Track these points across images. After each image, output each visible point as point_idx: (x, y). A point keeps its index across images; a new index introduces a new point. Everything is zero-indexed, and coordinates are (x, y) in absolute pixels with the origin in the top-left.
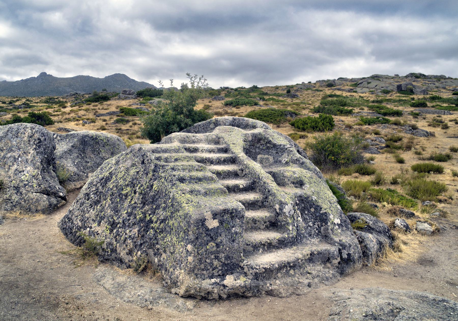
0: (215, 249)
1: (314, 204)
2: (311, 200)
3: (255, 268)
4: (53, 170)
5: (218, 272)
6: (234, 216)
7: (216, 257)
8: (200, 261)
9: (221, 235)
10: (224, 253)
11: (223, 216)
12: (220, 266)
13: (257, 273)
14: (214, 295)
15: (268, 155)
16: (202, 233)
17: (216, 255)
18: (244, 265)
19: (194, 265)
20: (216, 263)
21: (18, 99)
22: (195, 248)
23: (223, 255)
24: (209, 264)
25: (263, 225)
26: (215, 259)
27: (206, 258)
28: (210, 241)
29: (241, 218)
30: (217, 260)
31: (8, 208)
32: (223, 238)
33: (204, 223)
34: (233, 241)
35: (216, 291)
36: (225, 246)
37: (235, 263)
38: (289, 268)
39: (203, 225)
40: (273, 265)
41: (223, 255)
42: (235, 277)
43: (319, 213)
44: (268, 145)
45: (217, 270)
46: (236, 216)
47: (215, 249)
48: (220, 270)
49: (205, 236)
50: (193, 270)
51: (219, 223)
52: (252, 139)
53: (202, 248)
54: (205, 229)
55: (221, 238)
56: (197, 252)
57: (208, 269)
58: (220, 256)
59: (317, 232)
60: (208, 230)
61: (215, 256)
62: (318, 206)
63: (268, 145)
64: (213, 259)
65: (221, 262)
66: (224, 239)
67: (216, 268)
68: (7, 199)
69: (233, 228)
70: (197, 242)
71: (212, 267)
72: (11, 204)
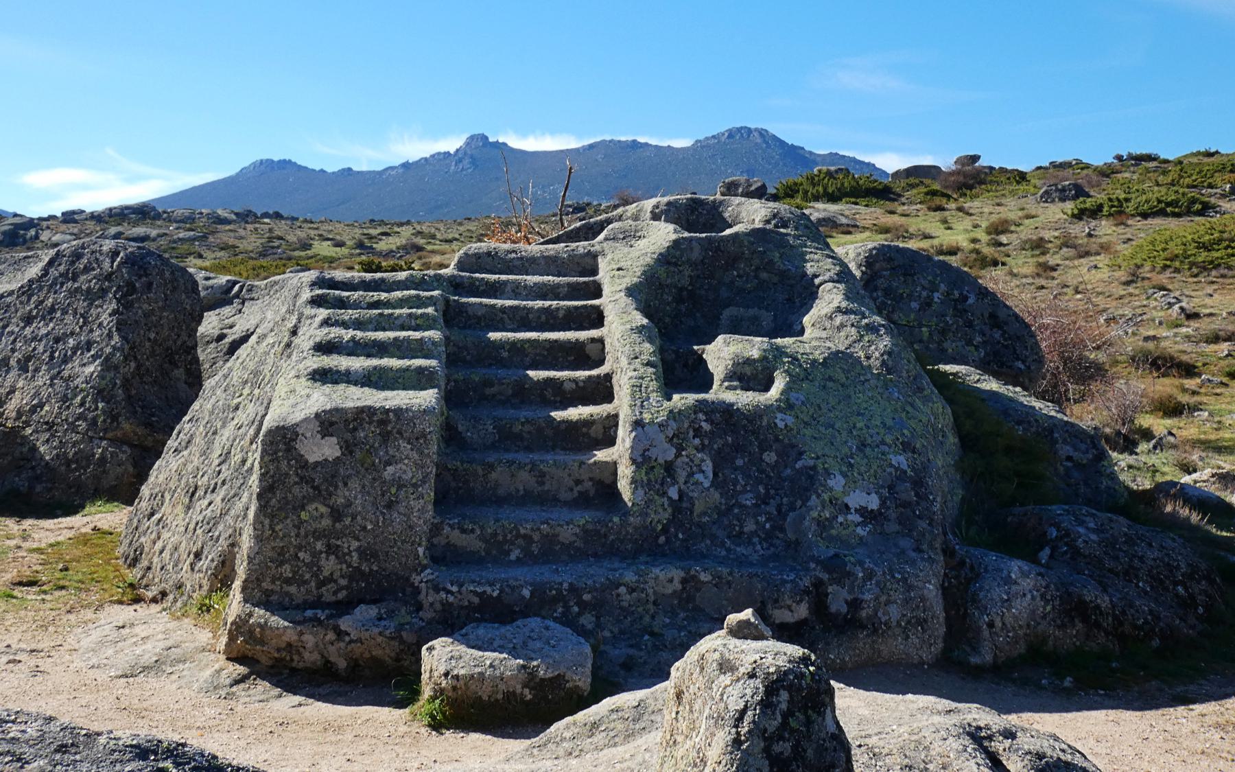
0: (326, 522)
1: (777, 440)
2: (769, 424)
3: (444, 589)
4: (186, 383)
5: (335, 593)
6: (391, 432)
7: (330, 549)
8: (279, 554)
9: (346, 484)
10: (359, 540)
11: (355, 429)
12: (342, 577)
13: (451, 604)
14: (306, 655)
15: (760, 308)
16: (287, 474)
17: (333, 541)
18: (422, 582)
19: (259, 564)
20: (329, 565)
21: (386, 229)
22: (264, 516)
23: (355, 544)
24: (307, 565)
25: (572, 490)
26: (326, 552)
27: (300, 547)
28: (312, 500)
29: (417, 439)
30: (332, 557)
31: (21, 483)
32: (352, 493)
33: (293, 444)
34: (390, 505)
35: (310, 645)
36: (359, 518)
37: (396, 574)
38: (576, 609)
39: (290, 449)
40: (513, 588)
41: (355, 544)
42: (383, 611)
43: (793, 468)
44: (764, 275)
45: (331, 586)
46: (399, 432)
47: (326, 522)
48: (342, 588)
49: (296, 483)
50: (258, 579)
51: (341, 448)
52: (704, 258)
53: (286, 518)
54: (296, 462)
55: (347, 493)
56: (270, 526)
57: (306, 582)
58: (346, 545)
59: (768, 526)
60: (303, 464)
61: (329, 546)
62: (793, 446)
63: (764, 275)
64: (321, 552)
65: (349, 566)
66: (356, 498)
67: (330, 579)
68: (23, 460)
69: (388, 468)
70: (271, 499)
71: (317, 576)
72: (30, 473)
